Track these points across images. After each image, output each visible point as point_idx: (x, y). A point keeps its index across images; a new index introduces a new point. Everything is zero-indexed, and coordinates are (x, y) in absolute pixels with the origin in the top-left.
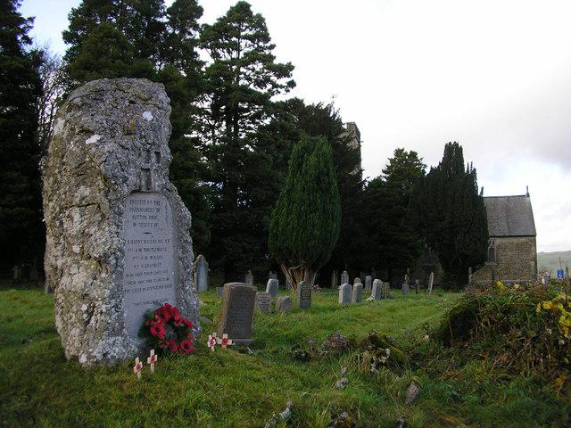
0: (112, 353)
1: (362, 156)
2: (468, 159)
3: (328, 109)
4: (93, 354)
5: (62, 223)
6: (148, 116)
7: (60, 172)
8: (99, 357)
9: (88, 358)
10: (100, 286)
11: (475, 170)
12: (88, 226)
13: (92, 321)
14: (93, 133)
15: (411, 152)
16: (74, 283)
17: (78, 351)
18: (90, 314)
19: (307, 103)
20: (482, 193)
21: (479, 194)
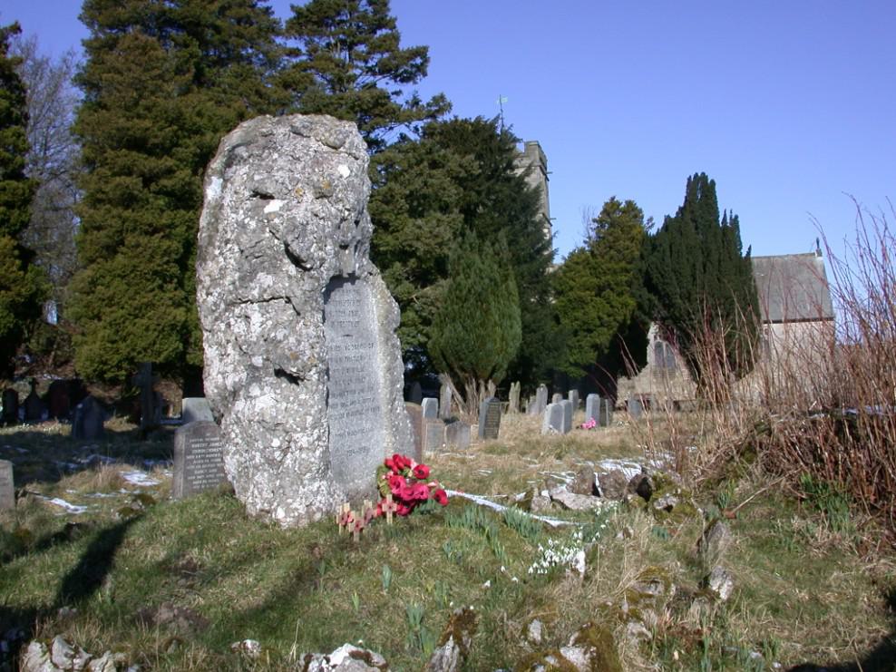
0: (318, 504)
1: (718, 200)
2: (727, 204)
3: (492, 126)
4: (294, 506)
5: (229, 325)
6: (344, 170)
7: (221, 254)
8: (302, 510)
9: (287, 512)
10: (297, 411)
11: (737, 217)
12: (275, 327)
13: (288, 461)
14: (272, 197)
15: (629, 204)
16: (257, 410)
17: (271, 504)
18: (285, 451)
19: (682, 205)
20: (749, 253)
21: (744, 255)
